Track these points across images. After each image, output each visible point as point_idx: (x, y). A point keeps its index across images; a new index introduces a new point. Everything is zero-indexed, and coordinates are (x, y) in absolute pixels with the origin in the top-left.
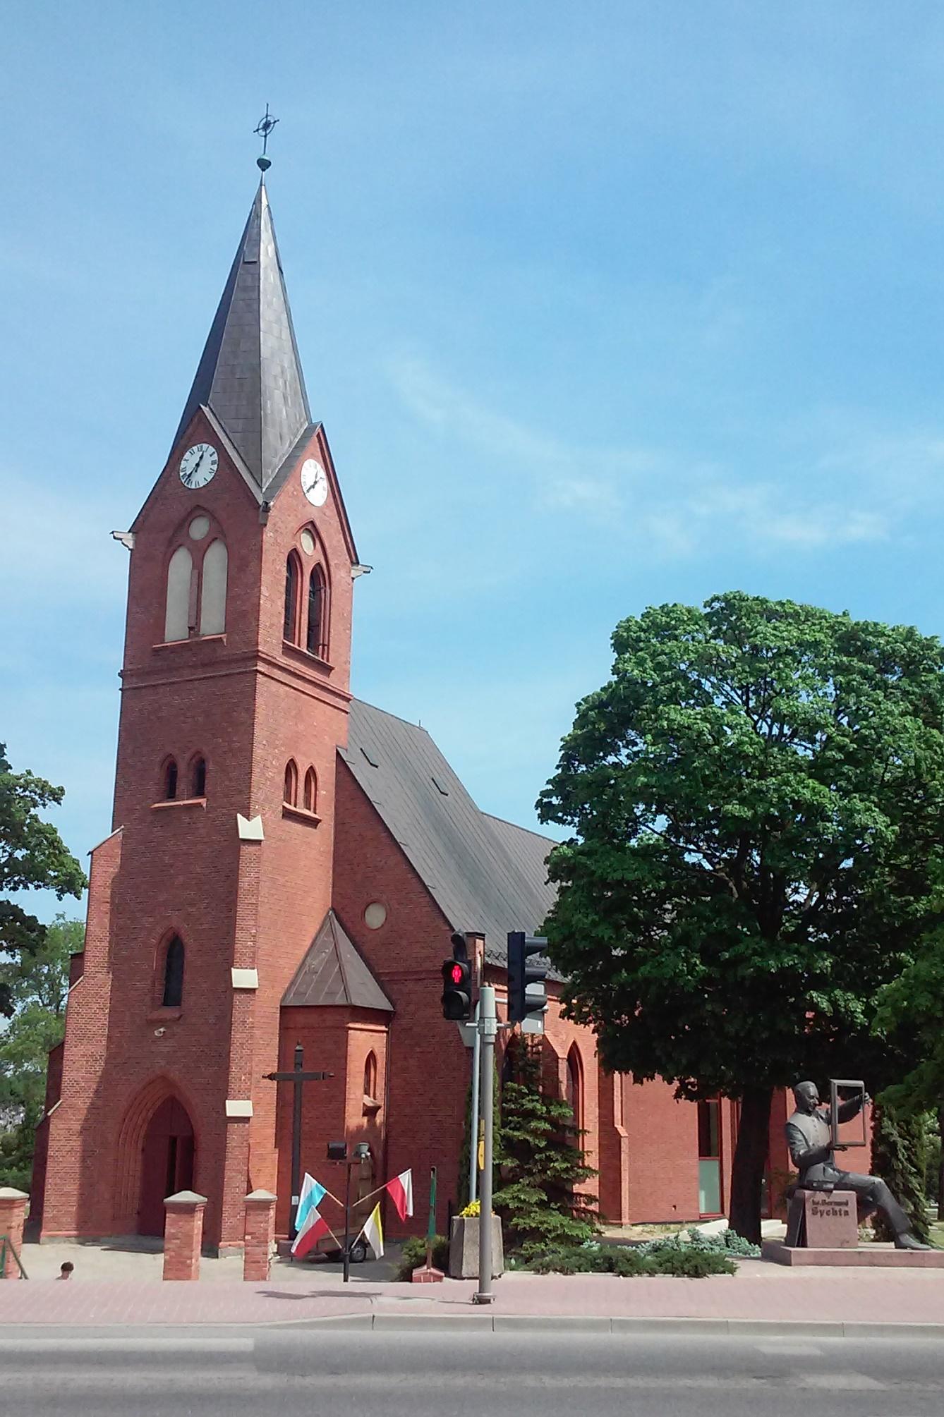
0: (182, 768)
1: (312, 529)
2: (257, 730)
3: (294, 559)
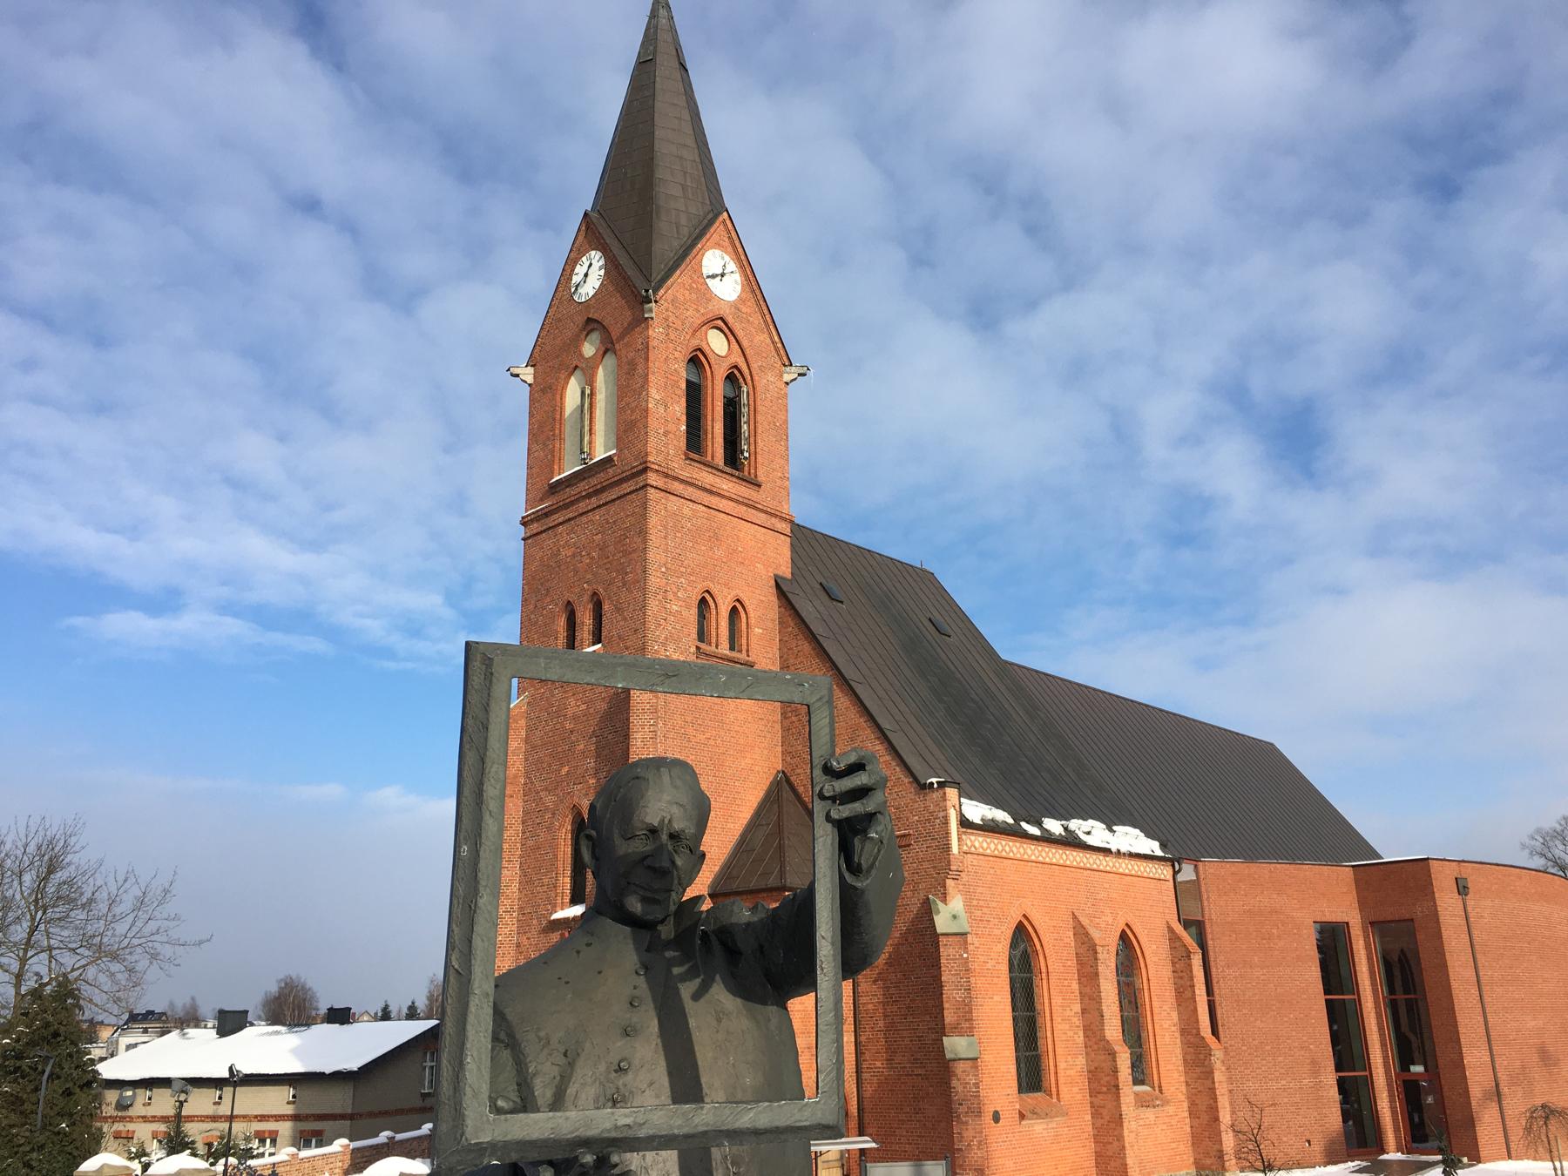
0: (860, 779)
1: (721, 324)
2: (651, 555)
3: (697, 361)
